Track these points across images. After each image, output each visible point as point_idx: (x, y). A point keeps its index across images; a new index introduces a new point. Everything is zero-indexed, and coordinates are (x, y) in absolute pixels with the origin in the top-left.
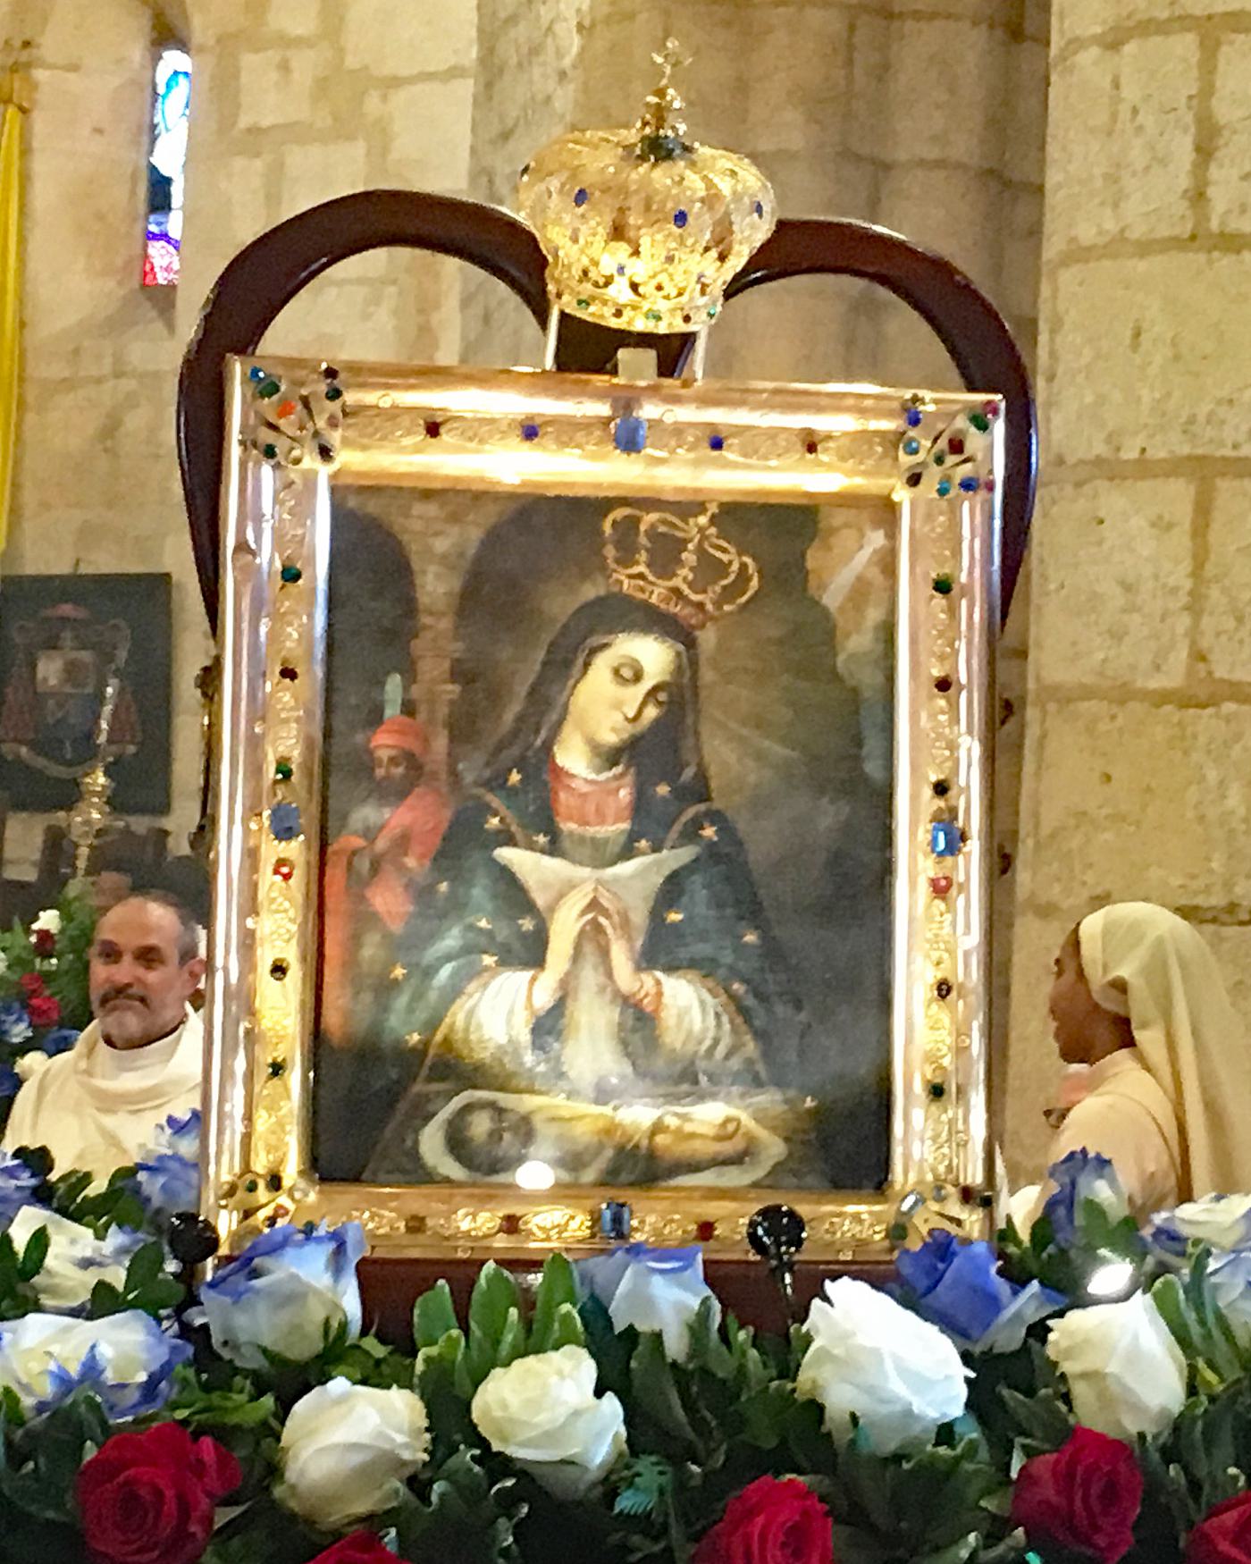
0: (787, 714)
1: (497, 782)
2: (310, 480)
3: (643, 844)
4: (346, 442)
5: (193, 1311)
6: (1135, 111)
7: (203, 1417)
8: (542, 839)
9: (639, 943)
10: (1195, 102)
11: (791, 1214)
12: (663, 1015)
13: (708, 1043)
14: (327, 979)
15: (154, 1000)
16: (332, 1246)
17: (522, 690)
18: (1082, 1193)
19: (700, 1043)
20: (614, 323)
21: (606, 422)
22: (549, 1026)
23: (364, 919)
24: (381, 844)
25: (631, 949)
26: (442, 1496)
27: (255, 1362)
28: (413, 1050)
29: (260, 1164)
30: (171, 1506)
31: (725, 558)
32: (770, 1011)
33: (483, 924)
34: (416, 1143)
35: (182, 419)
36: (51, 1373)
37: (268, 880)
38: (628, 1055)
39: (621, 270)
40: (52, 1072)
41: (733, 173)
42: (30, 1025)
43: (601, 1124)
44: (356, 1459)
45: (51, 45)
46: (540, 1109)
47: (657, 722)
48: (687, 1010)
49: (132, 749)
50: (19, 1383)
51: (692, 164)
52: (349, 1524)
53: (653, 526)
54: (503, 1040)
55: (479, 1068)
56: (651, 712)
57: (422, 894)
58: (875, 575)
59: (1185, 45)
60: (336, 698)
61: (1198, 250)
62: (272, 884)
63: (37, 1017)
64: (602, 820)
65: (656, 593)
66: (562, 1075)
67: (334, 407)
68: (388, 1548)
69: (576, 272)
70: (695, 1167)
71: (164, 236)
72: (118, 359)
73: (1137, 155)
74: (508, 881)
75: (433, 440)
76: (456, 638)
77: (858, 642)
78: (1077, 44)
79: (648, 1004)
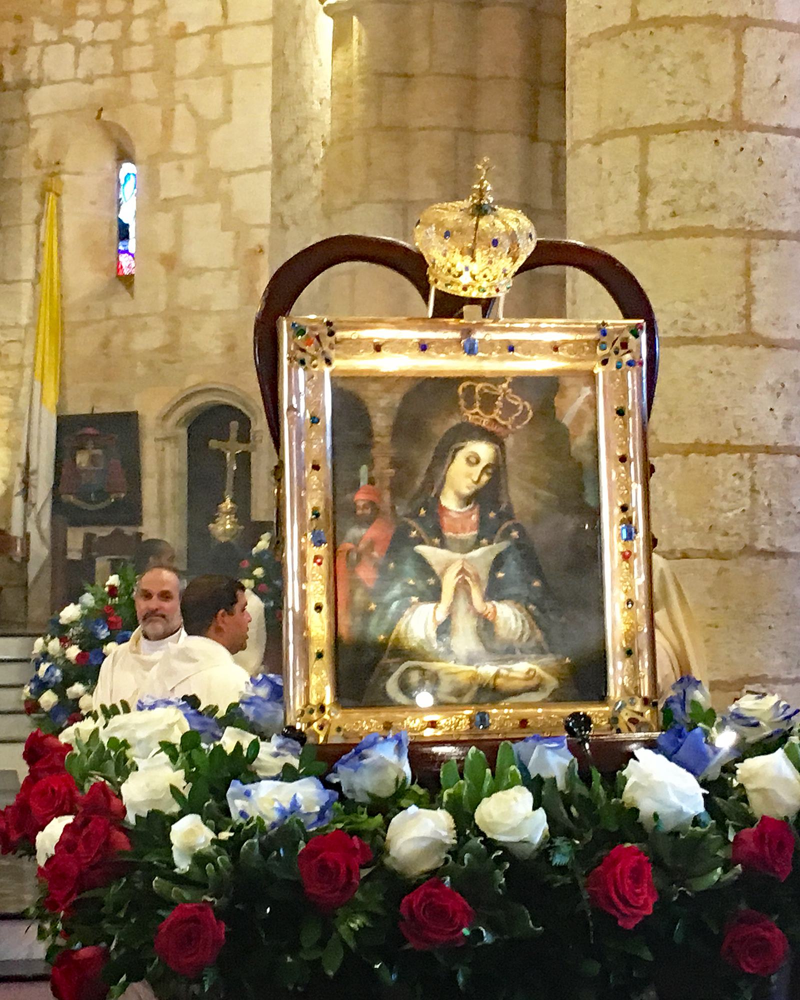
0: (548, 476)
1: (415, 515)
2: (321, 375)
3: (484, 541)
4: (337, 356)
5: (332, 775)
6: (610, 174)
7: (349, 827)
8: (437, 541)
10: (639, 169)
11: (585, 715)
12: (497, 622)
13: (519, 634)
14: (339, 612)
15: (169, 618)
16: (396, 742)
17: (424, 471)
18: (689, 698)
20: (463, 294)
22: (444, 629)
23: (355, 583)
24: (362, 546)
25: (481, 590)
26: (469, 860)
27: (366, 799)
29: (314, 701)
30: (343, 869)
31: (516, 403)
33: (411, 582)
34: (384, 688)
35: (257, 349)
36: (276, 809)
37: (311, 565)
40: (118, 653)
41: (517, 220)
42: (109, 629)
44: (424, 844)
45: (70, 162)
46: (442, 669)
47: (489, 482)
48: (509, 618)
49: (123, 495)
51: (497, 216)
52: (421, 875)
53: (482, 390)
54: (423, 637)
56: (485, 478)
57: (382, 569)
58: (586, 408)
59: (633, 141)
61: (642, 240)
62: (313, 567)
63: (111, 626)
64: (464, 529)
65: (485, 421)
67: (331, 339)
68: (447, 886)
69: (445, 271)
70: (516, 693)
71: (126, 252)
73: (611, 194)
74: (420, 559)
75: (378, 353)
77: (580, 441)
78: (579, 143)
79: (490, 617)
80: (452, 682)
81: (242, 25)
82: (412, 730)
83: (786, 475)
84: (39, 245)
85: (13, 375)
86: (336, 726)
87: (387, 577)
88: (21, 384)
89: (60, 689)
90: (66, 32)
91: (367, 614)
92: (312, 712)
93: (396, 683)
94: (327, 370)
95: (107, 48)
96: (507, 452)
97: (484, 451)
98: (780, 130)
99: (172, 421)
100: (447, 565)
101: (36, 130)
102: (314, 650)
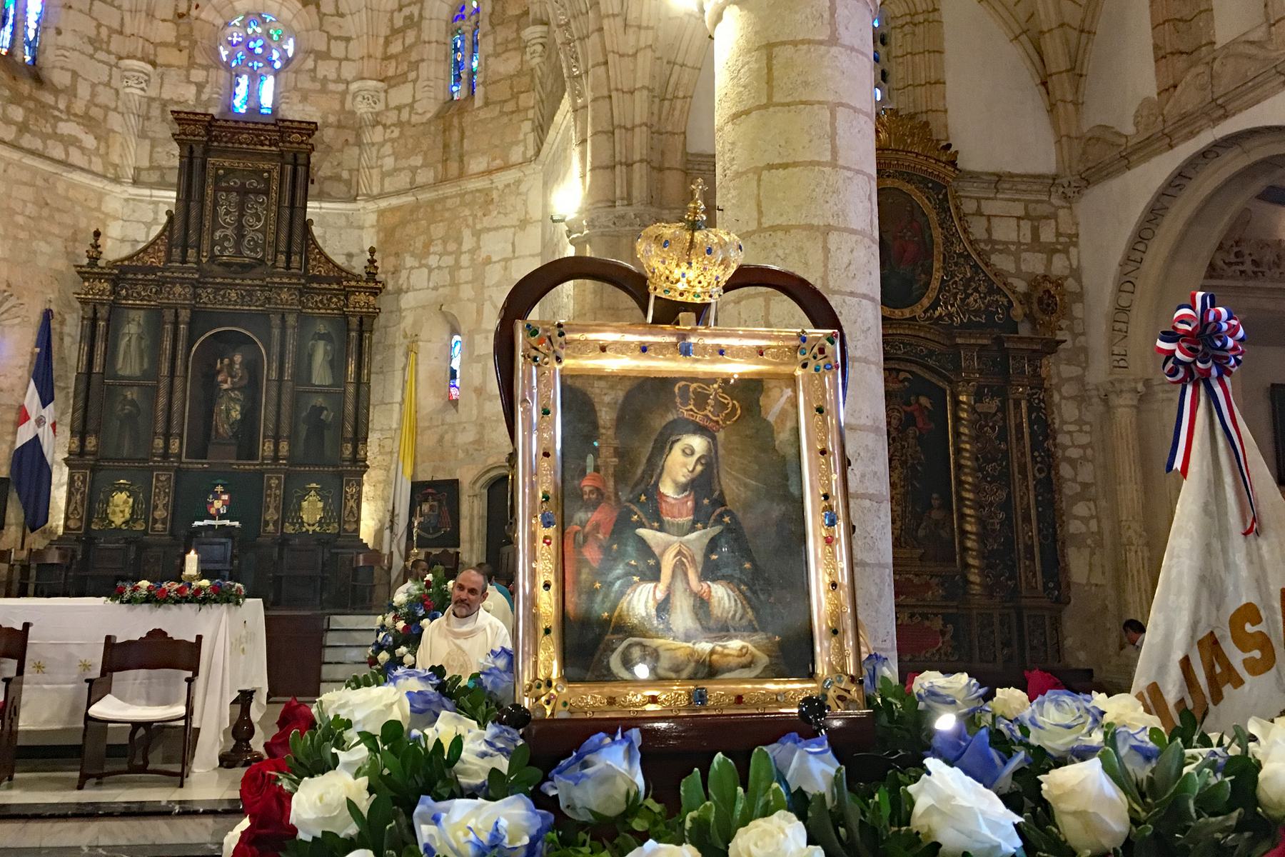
1: (636, 500)
3: (699, 525)
4: (568, 356)
5: (548, 784)
8: (656, 525)
9: (700, 570)
13: (732, 613)
16: (626, 744)
17: (644, 461)
18: (878, 674)
19: (729, 612)
20: (679, 299)
21: (676, 345)
22: (663, 607)
23: (582, 562)
24: (587, 529)
25: (697, 571)
28: (606, 620)
29: (541, 676)
32: (758, 597)
33: (633, 562)
34: (608, 662)
37: (540, 544)
38: (699, 619)
39: (683, 275)
43: (688, 651)
45: (423, 335)
46: (661, 645)
50: (452, 848)
55: (634, 627)
56: (699, 468)
57: (606, 550)
60: (566, 465)
64: (681, 515)
66: (670, 629)
67: (561, 339)
70: (730, 670)
71: (455, 386)
72: (443, 420)
74: (642, 541)
76: (616, 438)
77: (783, 436)
80: (670, 658)
81: (523, 257)
82: (635, 705)
83: (863, 512)
84: (404, 382)
85: (388, 458)
86: (562, 701)
87: (611, 558)
88: (391, 464)
89: (391, 650)
90: (423, 262)
91: (592, 592)
92: (539, 687)
93: (619, 659)
94: (558, 367)
95: (447, 271)
96: (719, 445)
97: (698, 443)
98: (852, 294)
99: (479, 485)
100: (667, 546)
101: (404, 317)
102: (542, 626)
